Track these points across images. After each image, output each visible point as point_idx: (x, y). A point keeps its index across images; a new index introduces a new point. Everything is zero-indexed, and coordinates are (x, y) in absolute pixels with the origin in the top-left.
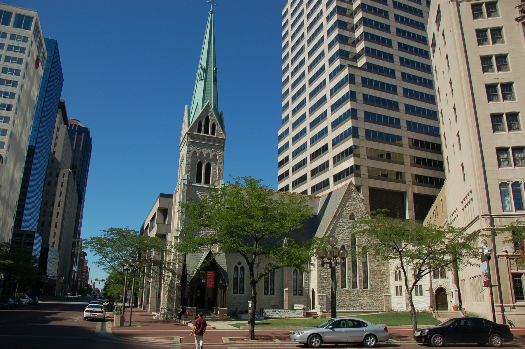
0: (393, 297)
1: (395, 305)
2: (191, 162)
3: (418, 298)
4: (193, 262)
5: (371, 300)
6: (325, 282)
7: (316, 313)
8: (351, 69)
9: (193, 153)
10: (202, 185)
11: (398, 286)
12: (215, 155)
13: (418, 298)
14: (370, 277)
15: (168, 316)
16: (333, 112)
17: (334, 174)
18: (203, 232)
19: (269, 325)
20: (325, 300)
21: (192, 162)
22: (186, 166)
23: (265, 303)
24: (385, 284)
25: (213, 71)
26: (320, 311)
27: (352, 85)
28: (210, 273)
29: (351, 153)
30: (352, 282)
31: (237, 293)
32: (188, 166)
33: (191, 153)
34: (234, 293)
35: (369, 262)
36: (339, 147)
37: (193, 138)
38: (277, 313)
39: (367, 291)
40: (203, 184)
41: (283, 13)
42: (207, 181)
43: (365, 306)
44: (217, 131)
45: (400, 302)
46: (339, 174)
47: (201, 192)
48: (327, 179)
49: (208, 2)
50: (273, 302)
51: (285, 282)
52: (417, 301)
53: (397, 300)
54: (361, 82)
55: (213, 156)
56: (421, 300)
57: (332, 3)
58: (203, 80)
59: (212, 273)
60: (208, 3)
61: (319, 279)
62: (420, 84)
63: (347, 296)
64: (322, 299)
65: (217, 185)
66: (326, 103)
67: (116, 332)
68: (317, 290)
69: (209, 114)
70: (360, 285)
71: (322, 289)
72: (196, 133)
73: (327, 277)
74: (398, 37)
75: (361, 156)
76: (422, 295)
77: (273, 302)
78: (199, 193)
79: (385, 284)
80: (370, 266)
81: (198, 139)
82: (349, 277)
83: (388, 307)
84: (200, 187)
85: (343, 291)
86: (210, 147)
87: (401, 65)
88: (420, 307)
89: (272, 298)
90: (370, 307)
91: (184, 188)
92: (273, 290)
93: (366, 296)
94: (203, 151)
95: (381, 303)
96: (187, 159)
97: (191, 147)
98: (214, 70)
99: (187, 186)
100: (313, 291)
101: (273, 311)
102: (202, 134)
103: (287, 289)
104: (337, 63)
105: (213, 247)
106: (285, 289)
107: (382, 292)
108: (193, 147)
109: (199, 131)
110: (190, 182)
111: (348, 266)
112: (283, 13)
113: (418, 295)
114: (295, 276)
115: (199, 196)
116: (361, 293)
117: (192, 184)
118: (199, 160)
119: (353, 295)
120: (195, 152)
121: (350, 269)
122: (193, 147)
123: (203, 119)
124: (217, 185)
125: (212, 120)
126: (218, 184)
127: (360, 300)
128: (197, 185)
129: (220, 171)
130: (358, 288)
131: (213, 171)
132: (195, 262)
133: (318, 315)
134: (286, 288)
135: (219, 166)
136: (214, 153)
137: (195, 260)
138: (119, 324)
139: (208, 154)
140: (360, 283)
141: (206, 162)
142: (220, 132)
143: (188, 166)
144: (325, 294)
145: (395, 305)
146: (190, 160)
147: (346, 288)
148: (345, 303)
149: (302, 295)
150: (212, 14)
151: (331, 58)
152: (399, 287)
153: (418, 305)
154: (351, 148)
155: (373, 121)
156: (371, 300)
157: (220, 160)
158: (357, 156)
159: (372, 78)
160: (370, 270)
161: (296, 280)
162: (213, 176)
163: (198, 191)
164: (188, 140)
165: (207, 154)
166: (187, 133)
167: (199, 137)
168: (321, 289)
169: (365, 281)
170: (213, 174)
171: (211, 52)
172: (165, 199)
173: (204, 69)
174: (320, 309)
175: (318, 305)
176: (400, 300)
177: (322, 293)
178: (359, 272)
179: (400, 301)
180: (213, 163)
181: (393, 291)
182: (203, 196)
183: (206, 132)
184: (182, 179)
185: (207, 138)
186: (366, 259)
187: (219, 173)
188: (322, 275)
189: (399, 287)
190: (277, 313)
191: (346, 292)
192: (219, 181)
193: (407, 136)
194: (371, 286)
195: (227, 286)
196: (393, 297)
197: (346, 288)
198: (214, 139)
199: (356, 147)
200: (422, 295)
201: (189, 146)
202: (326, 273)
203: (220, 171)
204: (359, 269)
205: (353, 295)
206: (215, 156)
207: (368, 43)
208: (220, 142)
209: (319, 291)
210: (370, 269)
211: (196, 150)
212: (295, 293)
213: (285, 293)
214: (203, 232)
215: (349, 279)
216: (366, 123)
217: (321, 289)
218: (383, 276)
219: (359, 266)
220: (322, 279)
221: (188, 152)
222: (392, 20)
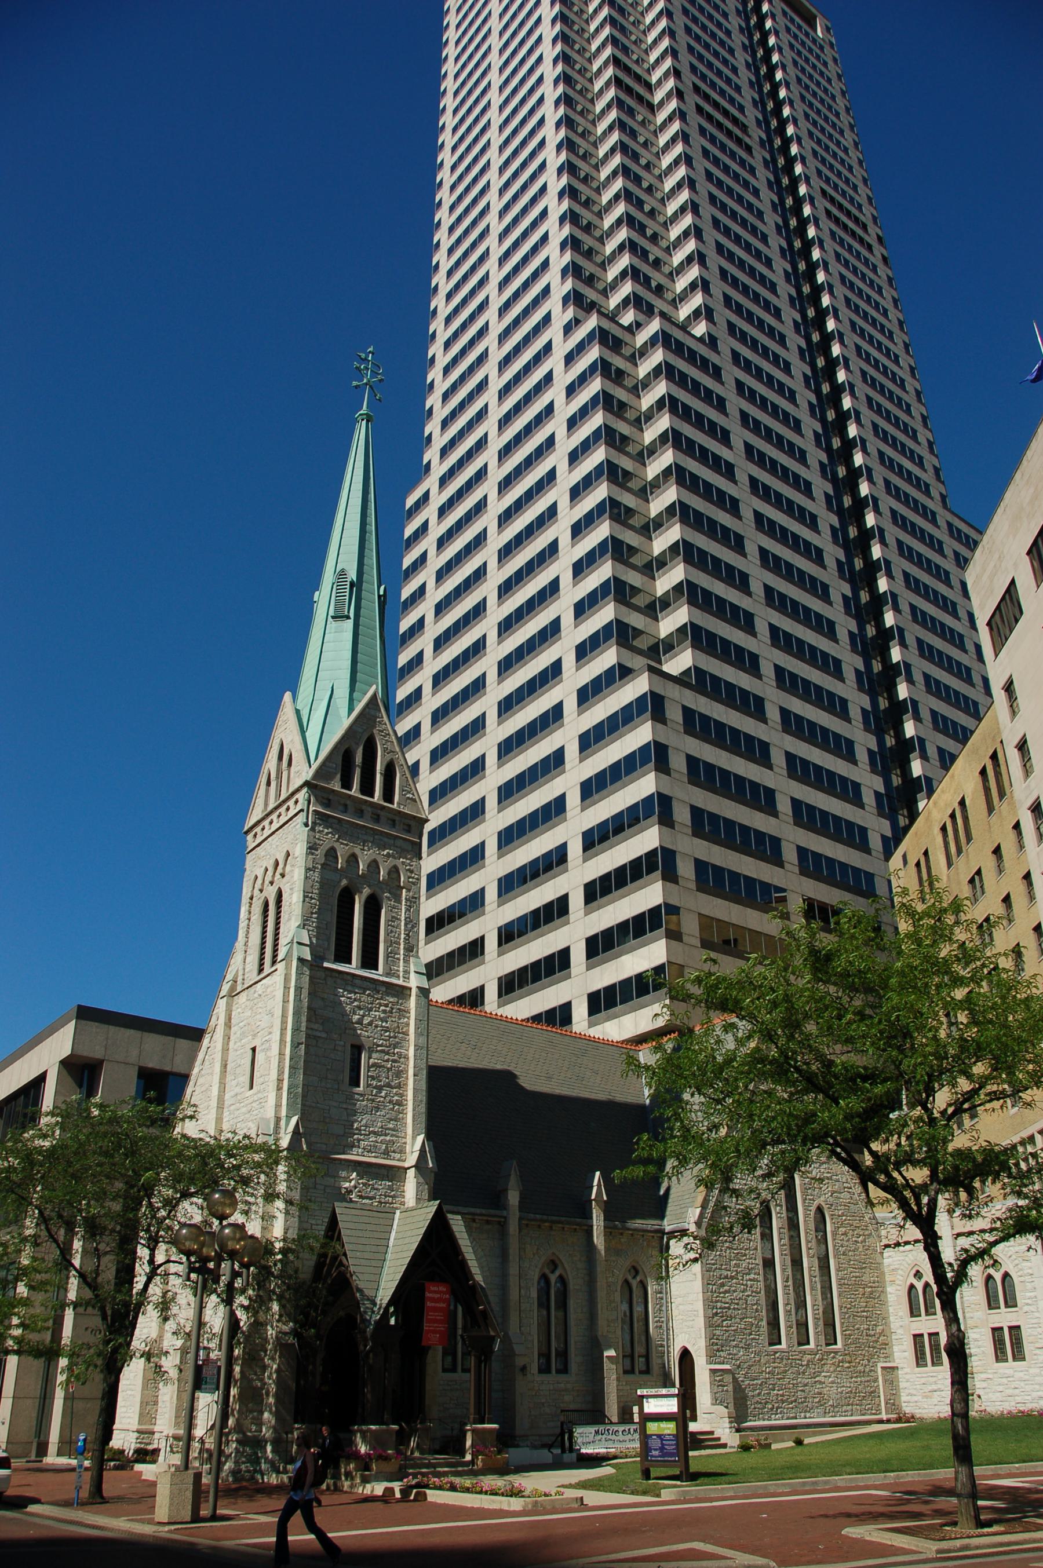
0: (906, 1370)
1: (915, 1398)
2: (320, 883)
3: (1007, 1371)
4: (368, 1248)
5: (847, 1384)
6: (725, 1323)
7: (712, 1433)
8: (656, 677)
9: (326, 855)
10: (353, 967)
11: (922, 1335)
12: (394, 871)
13: (1007, 1371)
14: (841, 1307)
15: (243, 1467)
16: (587, 801)
17: (590, 991)
18: (359, 1140)
19: (719, 1479)
20: (730, 1388)
21: (324, 884)
22: (305, 897)
23: (543, 1404)
24: (879, 1329)
25: (379, 596)
26: (728, 1425)
27: (659, 726)
28: (436, 1289)
29: (655, 925)
30: (794, 1322)
31: (454, 1370)
32: (312, 898)
33: (320, 853)
34: (444, 1370)
35: (835, 1257)
36: (610, 908)
37: (327, 803)
38: (610, 1437)
39: (836, 1353)
40: (357, 968)
41: (410, 502)
42: (370, 960)
43: (832, 1406)
44: (402, 790)
45: (935, 1387)
46: (610, 990)
47: (352, 995)
48: (561, 1006)
49: (355, 383)
50: (567, 1398)
51: (602, 1327)
52: (1005, 1380)
53: (923, 1380)
54: (680, 720)
55: (389, 873)
56: (1021, 1374)
57: (591, 488)
58: (348, 617)
59: (441, 1288)
60: (357, 387)
61: (710, 1313)
62: (824, 746)
63: (785, 1372)
64: (721, 1384)
65: (401, 974)
66: (564, 772)
67: (435, 1540)
68: (703, 1352)
69: (375, 731)
70: (816, 1333)
71: (718, 1350)
72: (336, 785)
73: (729, 1308)
74: (769, 609)
75: (685, 938)
76: (1024, 1359)
77: (567, 1398)
78: (345, 997)
79: (879, 1329)
80: (838, 1270)
81: (341, 808)
82: (788, 1308)
83: (894, 1404)
84: (349, 977)
85: (776, 1353)
86: (381, 841)
87: (778, 687)
88: (1018, 1399)
89: (562, 1385)
90: (850, 1407)
91: (299, 974)
92: (563, 1355)
93: (835, 1371)
94: (357, 851)
95: (873, 1393)
96: (306, 872)
97: (320, 832)
98: (382, 593)
99: (311, 970)
100: (686, 1356)
101: (597, 1432)
102: (355, 791)
103: (612, 1353)
104: (608, 657)
105: (393, 1197)
106: (606, 1354)
107: (872, 1356)
108: (327, 834)
109: (347, 784)
110: (318, 957)
111: (783, 1270)
112: (410, 502)
113: (1006, 1361)
114: (625, 1307)
115: (348, 1008)
116: (822, 1359)
117: (326, 964)
118: (344, 882)
119: (802, 1369)
120: (331, 853)
121: (787, 1281)
122: (327, 834)
123: (358, 744)
124: (401, 974)
125: (385, 750)
126: (407, 972)
127: (821, 1382)
128: (340, 968)
129: (409, 926)
130: (812, 1345)
131: (387, 925)
132: (374, 1249)
133: (719, 1439)
134: (609, 1347)
135: (407, 910)
136: (391, 862)
137: (373, 1242)
138: (187, 1514)
139: (374, 865)
140: (816, 1326)
141: (366, 891)
142: (410, 796)
143: (312, 898)
144: (727, 1367)
145: (915, 1398)
146: (316, 876)
147: (780, 1343)
148: (782, 1395)
149: (647, 1371)
150: (368, 421)
151: (438, 673)
152: (926, 1337)
153: (1010, 1392)
154: (655, 912)
155: (713, 837)
156: (847, 1384)
157: (409, 890)
158: (674, 935)
159: (708, 713)
160: (840, 1285)
161: (628, 1319)
162: (389, 943)
163: (345, 990)
164: (312, 808)
165: (369, 866)
166: (306, 784)
167: (345, 804)
168: (715, 1347)
169: (830, 1324)
170: (387, 934)
171: (370, 537)
172: (93, 1027)
173: (352, 584)
174: (727, 1420)
175: (713, 1404)
176: (934, 1379)
177: (720, 1363)
178: (812, 1289)
179: (935, 1383)
180: (388, 899)
181: (902, 1353)
182: (359, 1008)
183: (367, 788)
184: (292, 942)
185: (369, 809)
186: (824, 1247)
187: (408, 935)
188: (717, 1302)
189: (926, 1337)
190: (610, 1437)
191: (782, 1359)
192: (406, 961)
193: (799, 891)
194: (846, 1337)
195: (492, 1339)
196: (906, 1370)
197: (780, 1343)
198: (390, 816)
199: (672, 909)
200: (1024, 1359)
201: (313, 829)
202: (726, 1292)
203: (409, 926)
204: (811, 1281)
205: (802, 1369)
206: (394, 876)
207: (697, 612)
208: (408, 830)
209: (712, 1355)
210: (839, 1280)
211: (337, 845)
212: (629, 1368)
213: (607, 1365)
214: (359, 1140)
215: (788, 1313)
216: (697, 841)
217: (715, 1347)
218: (872, 1302)
219: (810, 1268)
220: (716, 1314)
221: (309, 848)
222: (754, 560)
